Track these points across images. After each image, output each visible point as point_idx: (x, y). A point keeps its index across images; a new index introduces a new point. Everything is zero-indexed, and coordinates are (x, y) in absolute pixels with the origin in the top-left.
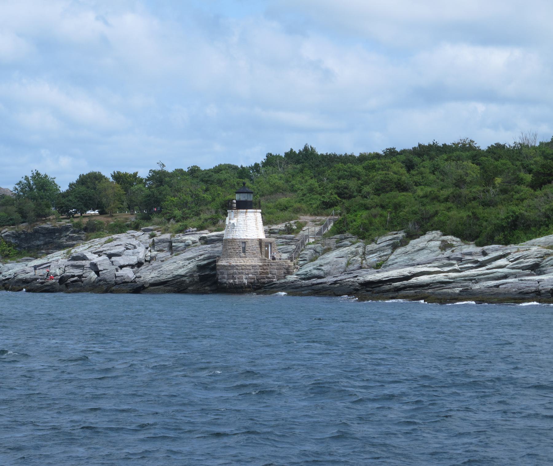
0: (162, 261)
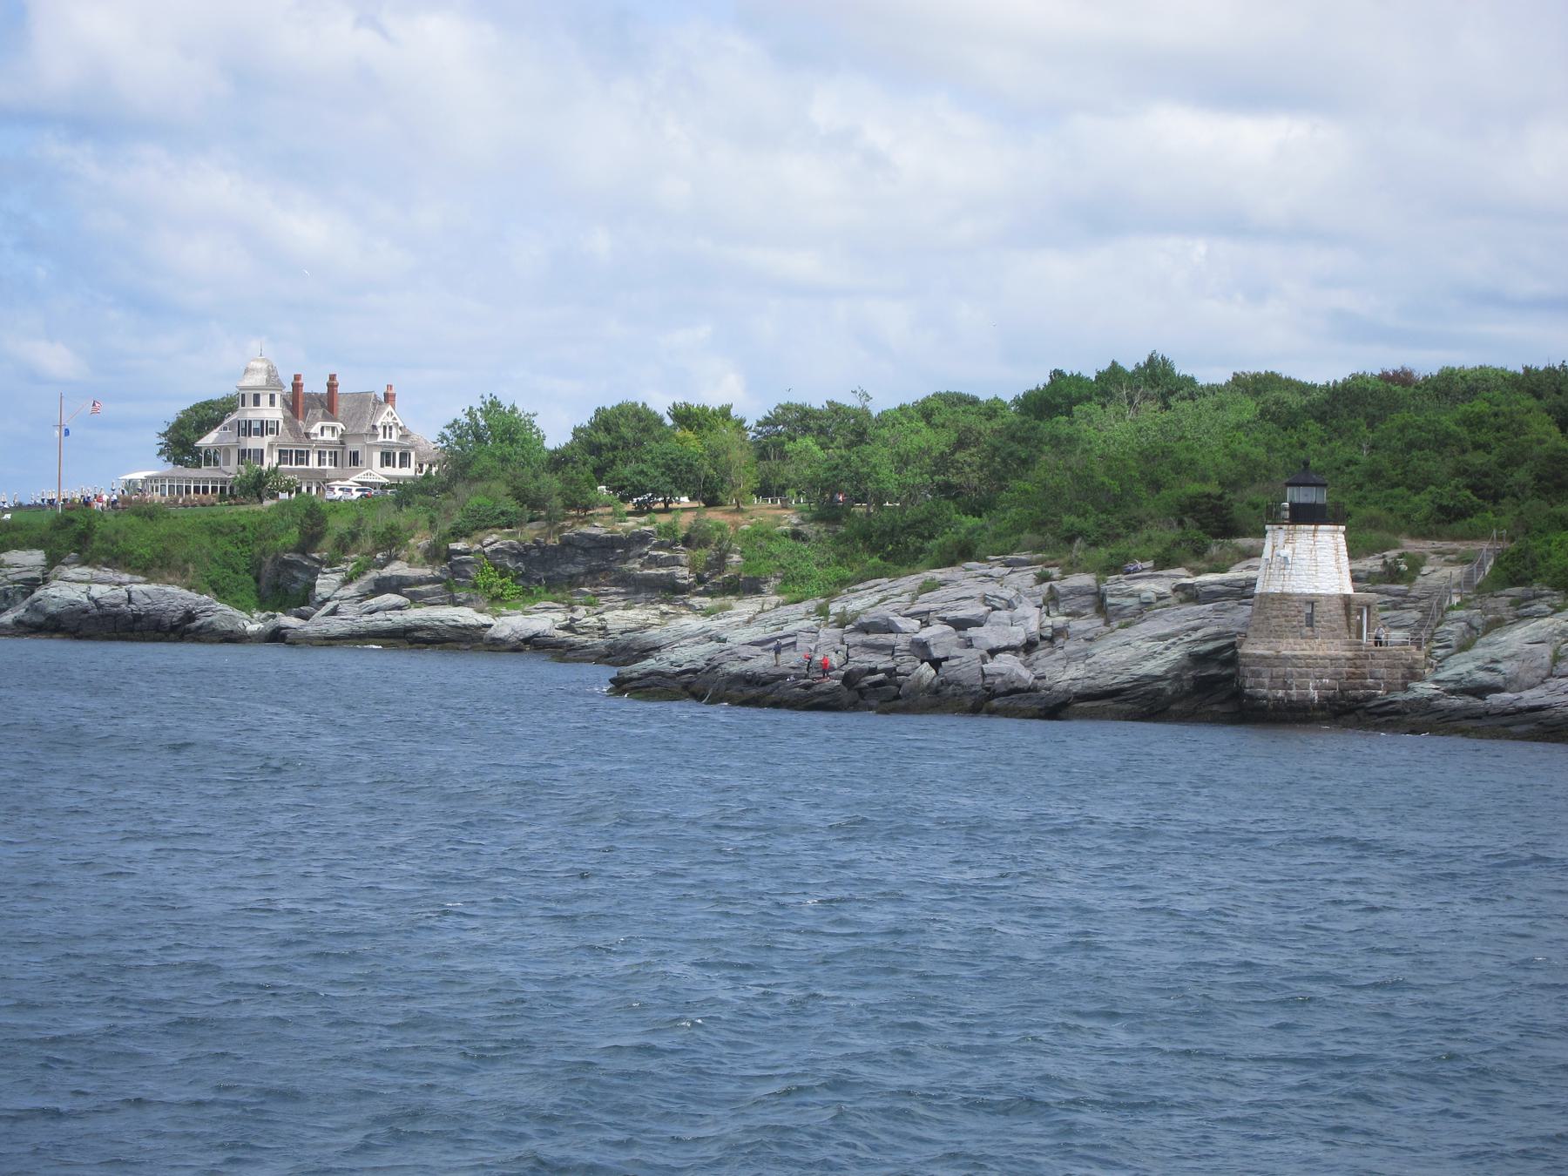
0: (1091, 640)
